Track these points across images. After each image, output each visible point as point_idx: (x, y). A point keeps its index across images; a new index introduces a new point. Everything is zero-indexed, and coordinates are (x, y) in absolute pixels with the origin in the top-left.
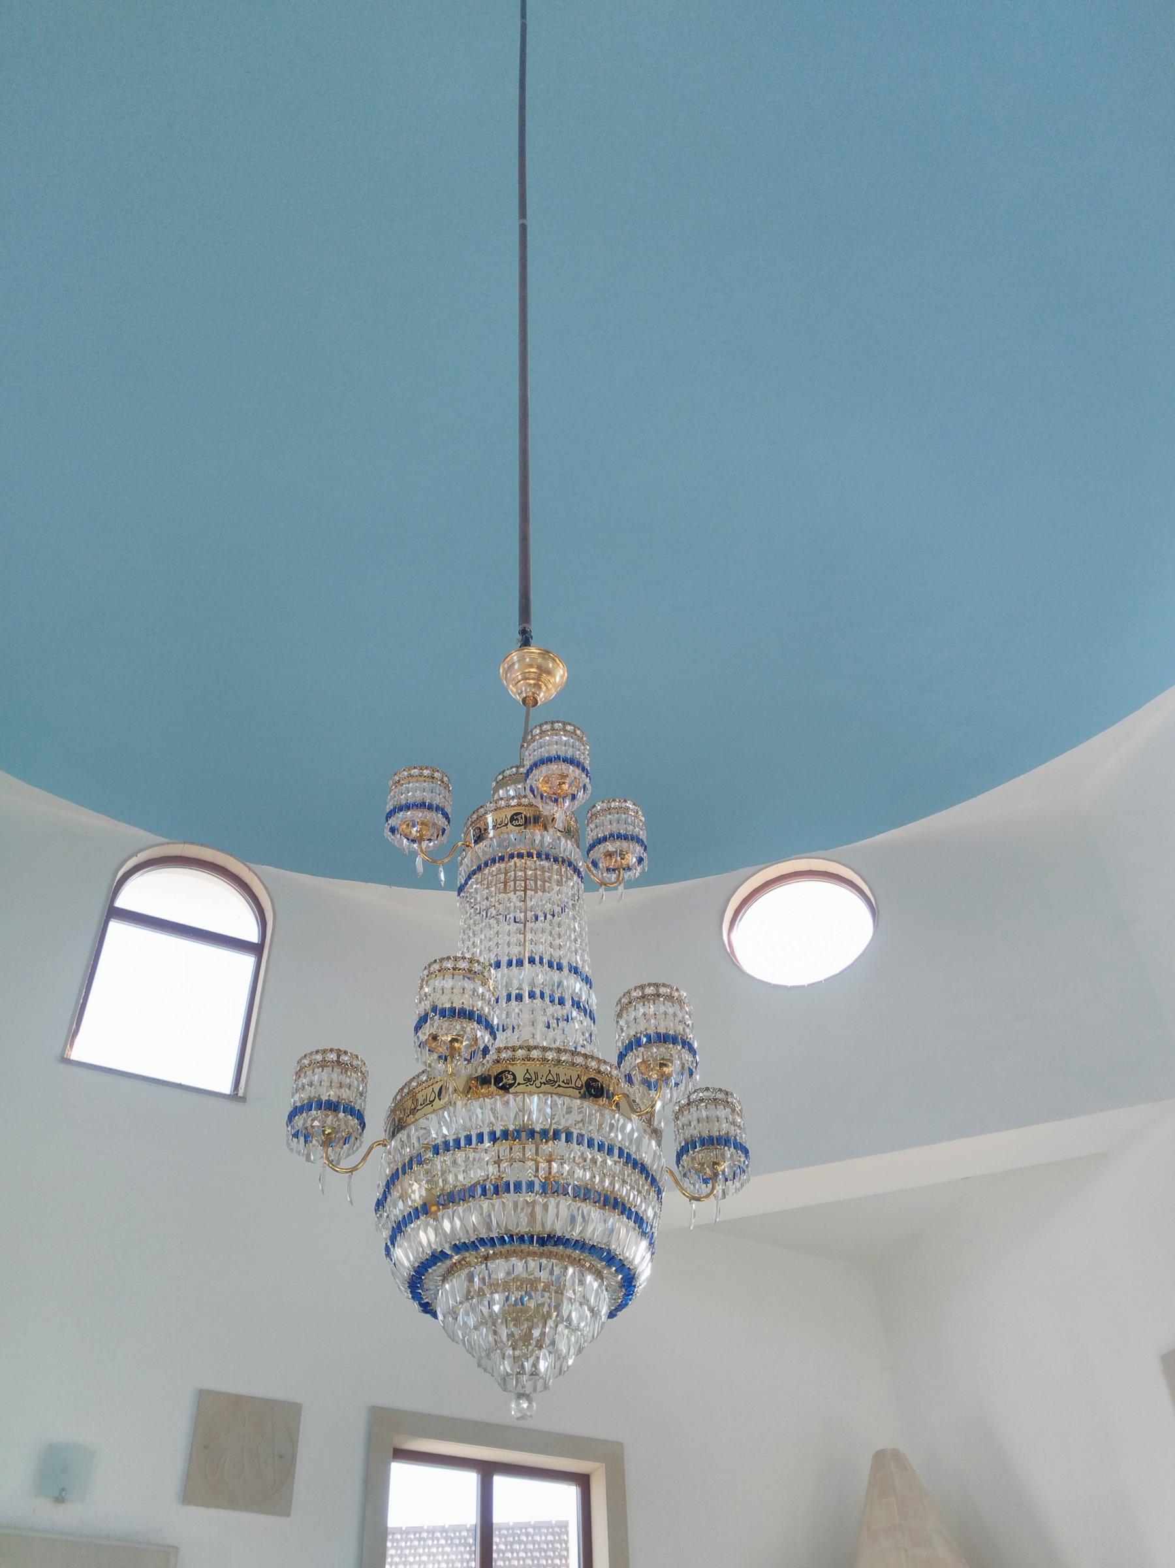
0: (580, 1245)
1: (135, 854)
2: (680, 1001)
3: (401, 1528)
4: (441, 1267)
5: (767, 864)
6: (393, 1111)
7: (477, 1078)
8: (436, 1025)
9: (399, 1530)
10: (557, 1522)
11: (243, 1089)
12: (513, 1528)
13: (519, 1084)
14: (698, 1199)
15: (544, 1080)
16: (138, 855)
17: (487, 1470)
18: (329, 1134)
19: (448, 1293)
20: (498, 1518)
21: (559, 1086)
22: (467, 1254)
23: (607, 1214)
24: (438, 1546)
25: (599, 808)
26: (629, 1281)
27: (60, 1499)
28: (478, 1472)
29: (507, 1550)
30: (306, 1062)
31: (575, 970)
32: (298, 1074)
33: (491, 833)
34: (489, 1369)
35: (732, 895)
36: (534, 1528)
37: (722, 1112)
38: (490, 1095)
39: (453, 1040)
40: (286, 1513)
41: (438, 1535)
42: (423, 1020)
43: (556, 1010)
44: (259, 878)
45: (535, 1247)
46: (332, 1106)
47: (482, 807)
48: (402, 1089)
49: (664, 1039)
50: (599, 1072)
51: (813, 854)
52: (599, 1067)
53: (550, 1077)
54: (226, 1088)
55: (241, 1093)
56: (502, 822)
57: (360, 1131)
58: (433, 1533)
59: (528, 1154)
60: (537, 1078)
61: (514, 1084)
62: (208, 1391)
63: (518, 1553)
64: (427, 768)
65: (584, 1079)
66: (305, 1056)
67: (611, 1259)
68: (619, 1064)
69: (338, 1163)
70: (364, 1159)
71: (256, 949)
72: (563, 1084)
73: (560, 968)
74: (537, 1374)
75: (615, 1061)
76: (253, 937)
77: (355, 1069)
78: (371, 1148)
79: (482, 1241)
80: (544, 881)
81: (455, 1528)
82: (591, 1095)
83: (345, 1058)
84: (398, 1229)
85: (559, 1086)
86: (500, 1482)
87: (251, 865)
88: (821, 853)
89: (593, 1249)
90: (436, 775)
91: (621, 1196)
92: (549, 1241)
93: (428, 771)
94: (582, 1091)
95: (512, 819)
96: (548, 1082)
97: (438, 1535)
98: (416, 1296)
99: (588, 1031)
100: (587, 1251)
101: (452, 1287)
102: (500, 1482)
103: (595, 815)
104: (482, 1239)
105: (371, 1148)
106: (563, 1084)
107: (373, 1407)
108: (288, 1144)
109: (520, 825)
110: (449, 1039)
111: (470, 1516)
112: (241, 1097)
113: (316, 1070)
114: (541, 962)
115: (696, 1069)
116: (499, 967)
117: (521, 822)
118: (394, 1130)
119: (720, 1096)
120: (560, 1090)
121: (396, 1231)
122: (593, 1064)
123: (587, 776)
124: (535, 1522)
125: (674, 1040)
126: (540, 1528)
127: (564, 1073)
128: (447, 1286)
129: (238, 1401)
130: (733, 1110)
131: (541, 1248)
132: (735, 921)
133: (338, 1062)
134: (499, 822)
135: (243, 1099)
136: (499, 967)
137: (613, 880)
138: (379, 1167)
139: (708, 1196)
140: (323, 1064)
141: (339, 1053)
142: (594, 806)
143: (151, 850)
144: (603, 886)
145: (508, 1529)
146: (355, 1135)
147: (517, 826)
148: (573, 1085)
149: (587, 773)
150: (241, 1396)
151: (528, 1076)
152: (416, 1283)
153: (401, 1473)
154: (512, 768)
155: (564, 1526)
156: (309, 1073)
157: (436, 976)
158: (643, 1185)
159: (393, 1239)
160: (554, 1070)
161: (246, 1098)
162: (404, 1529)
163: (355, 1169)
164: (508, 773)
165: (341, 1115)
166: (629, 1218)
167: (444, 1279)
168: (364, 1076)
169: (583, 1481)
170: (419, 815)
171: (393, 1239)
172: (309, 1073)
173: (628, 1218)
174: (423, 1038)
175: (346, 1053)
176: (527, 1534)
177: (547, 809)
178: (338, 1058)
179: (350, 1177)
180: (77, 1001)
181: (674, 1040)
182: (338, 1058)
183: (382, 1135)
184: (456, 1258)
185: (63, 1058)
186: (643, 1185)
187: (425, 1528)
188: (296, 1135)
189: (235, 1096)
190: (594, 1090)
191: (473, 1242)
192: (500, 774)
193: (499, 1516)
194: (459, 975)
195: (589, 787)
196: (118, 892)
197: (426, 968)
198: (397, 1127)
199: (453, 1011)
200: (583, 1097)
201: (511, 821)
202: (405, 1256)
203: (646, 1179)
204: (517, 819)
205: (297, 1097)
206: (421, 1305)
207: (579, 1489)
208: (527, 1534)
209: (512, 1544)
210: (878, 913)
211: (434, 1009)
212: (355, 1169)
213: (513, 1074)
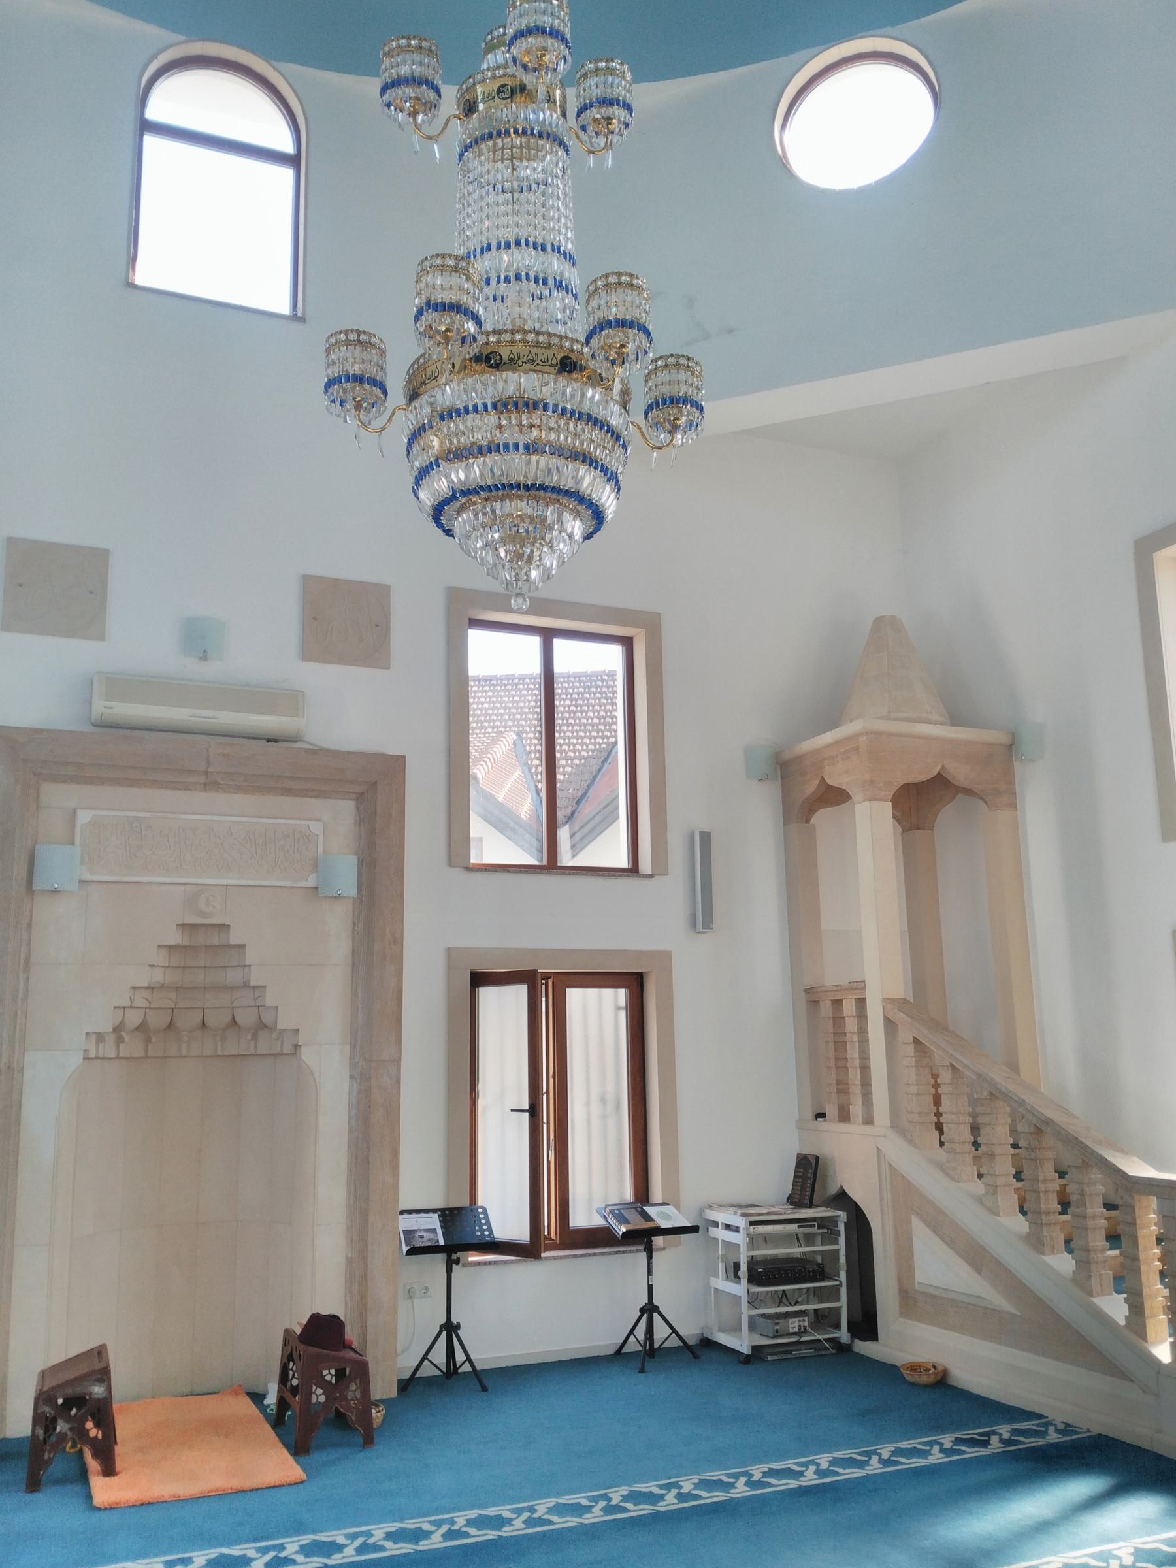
0: (556, 490)
1: (154, 57)
2: (639, 289)
3: (496, 676)
4: (455, 505)
5: (830, 45)
6: (409, 382)
7: (471, 359)
8: (430, 316)
9: (488, 680)
10: (573, 673)
11: (301, 309)
12: (590, 676)
13: (505, 363)
14: (660, 448)
15: (525, 360)
16: (159, 57)
17: (548, 636)
18: (359, 401)
19: (462, 522)
20: (558, 669)
21: (538, 364)
22: (471, 497)
23: (578, 465)
24: (527, 689)
25: (587, 68)
26: (598, 516)
27: (204, 658)
28: (540, 637)
29: (585, 693)
30: (333, 340)
31: (557, 249)
32: (328, 351)
33: (481, 107)
34: (495, 576)
35: (787, 85)
36: (575, 677)
37: (683, 376)
38: (482, 373)
39: (448, 330)
40: (387, 667)
41: (528, 681)
42: (420, 312)
43: (538, 290)
44: (285, 78)
45: (522, 492)
46: (359, 379)
47: (470, 77)
48: (413, 364)
49: (621, 324)
50: (572, 350)
51: (879, 32)
52: (572, 346)
53: (530, 357)
54: (285, 309)
55: (299, 314)
56: (489, 94)
57: (383, 398)
58: (524, 679)
59: (514, 422)
60: (519, 358)
61: (500, 363)
62: (310, 576)
63: (594, 695)
64: (414, 38)
65: (559, 357)
66: (332, 335)
67: (581, 499)
68: (588, 341)
69: (370, 424)
70: (390, 420)
71: (293, 161)
72: (540, 363)
73: (544, 249)
74: (528, 581)
75: (583, 339)
76: (288, 147)
77: (373, 346)
78: (394, 413)
79: (482, 488)
80: (538, 150)
81: (522, 678)
82: (565, 371)
83: (363, 337)
84: (424, 473)
85: (538, 364)
86: (558, 644)
87: (275, 63)
88: (888, 30)
89: (567, 493)
90: (425, 44)
91: (589, 452)
92: (531, 489)
93: (417, 41)
94: (557, 368)
95: (499, 92)
96: (528, 361)
97: (528, 681)
98: (439, 524)
99: (569, 308)
100: (562, 494)
101: (463, 519)
102: (558, 644)
103: (585, 76)
104: (482, 486)
105: (394, 413)
106: (540, 363)
107: (449, 587)
108: (328, 409)
109: (506, 98)
110: (444, 329)
111: (535, 667)
112: (300, 317)
113: (341, 348)
114: (527, 244)
115: (649, 348)
116: (490, 250)
117: (508, 94)
118: (410, 398)
119: (683, 361)
120: (538, 368)
121: (423, 474)
122: (568, 344)
123: (567, 46)
124: (591, 672)
125: (631, 325)
126: (524, 679)
127: (542, 353)
128: (460, 519)
129: (336, 583)
130: (693, 373)
131: (527, 493)
132: (790, 113)
133: (359, 340)
134: (486, 94)
135: (302, 320)
136: (490, 250)
137: (602, 145)
138: (405, 422)
139: (667, 445)
140: (347, 342)
141: (359, 333)
142: (583, 66)
143: (170, 51)
144: (591, 155)
145: (564, 677)
146: (379, 402)
147: (503, 99)
148: (550, 363)
149: (567, 42)
150: (338, 580)
151: (512, 356)
152: (437, 513)
153: (477, 638)
154: (499, 27)
155: (612, 675)
156: (336, 350)
157: (428, 272)
158: (608, 443)
159: (417, 483)
160: (534, 350)
161: (305, 318)
162: (517, 675)
163: (384, 428)
164: (495, 33)
165: (367, 387)
166: (596, 468)
167: (459, 512)
168: (382, 353)
169: (628, 643)
170: (410, 91)
171: (417, 483)
172: (336, 350)
173: (595, 468)
174: (422, 329)
175: (364, 332)
176: (602, 681)
177: (528, 79)
178: (359, 337)
179: (379, 436)
180: (130, 224)
181: (631, 325)
182: (359, 337)
183: (402, 401)
184: (463, 500)
185: (128, 283)
186: (608, 443)
187: (517, 675)
188: (333, 401)
189: (296, 317)
190: (568, 366)
191: (475, 489)
192: (488, 34)
193: (558, 668)
194: (447, 271)
195: (569, 58)
196: (146, 100)
197: (419, 264)
198: (413, 395)
199: (443, 305)
200: (559, 372)
201: (498, 94)
202: (427, 497)
203: (612, 436)
204: (503, 92)
205: (330, 371)
206: (444, 531)
207: (624, 648)
208: (602, 681)
209: (589, 688)
210: (941, 102)
211: (428, 303)
212: (384, 428)
213: (500, 355)
